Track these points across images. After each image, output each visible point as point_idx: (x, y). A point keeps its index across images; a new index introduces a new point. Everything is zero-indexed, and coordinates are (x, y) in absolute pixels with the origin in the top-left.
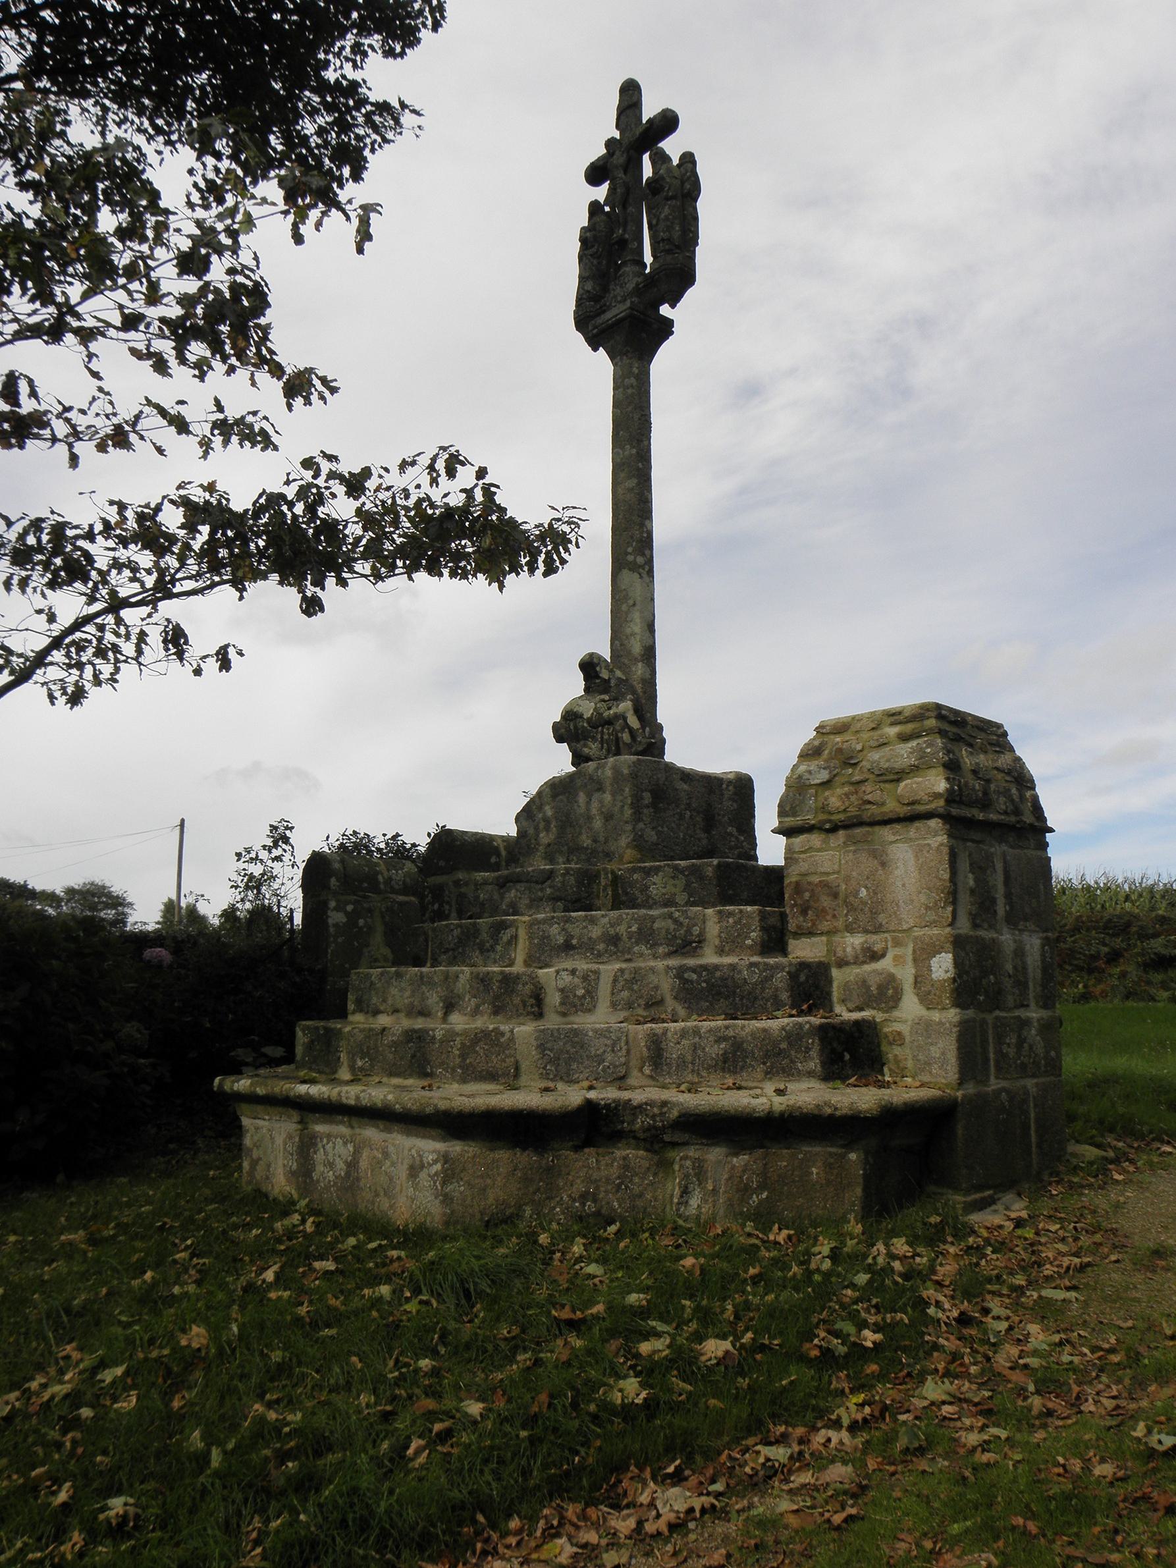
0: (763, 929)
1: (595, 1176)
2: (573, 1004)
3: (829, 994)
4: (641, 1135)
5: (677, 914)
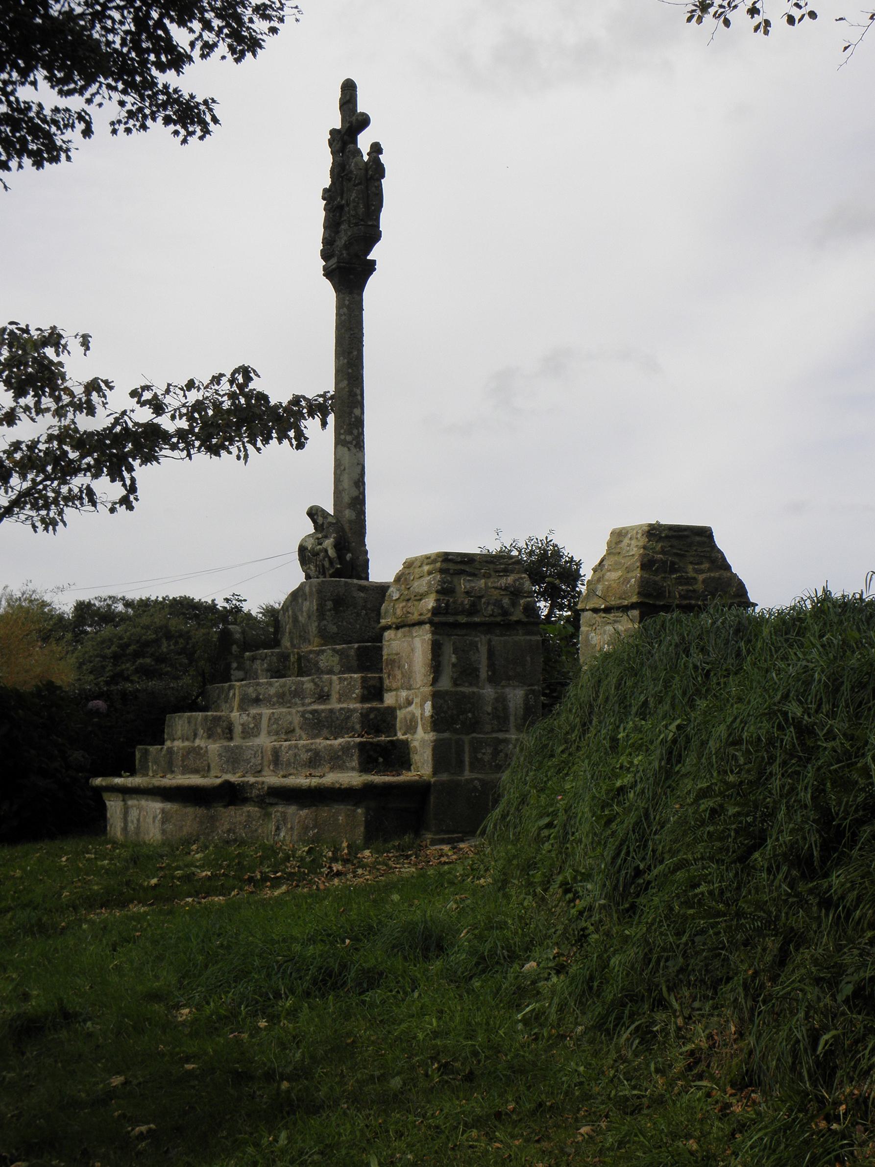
0: (363, 687)
1: (234, 821)
2: (248, 733)
3: (394, 725)
4: (256, 800)
5: (317, 680)
